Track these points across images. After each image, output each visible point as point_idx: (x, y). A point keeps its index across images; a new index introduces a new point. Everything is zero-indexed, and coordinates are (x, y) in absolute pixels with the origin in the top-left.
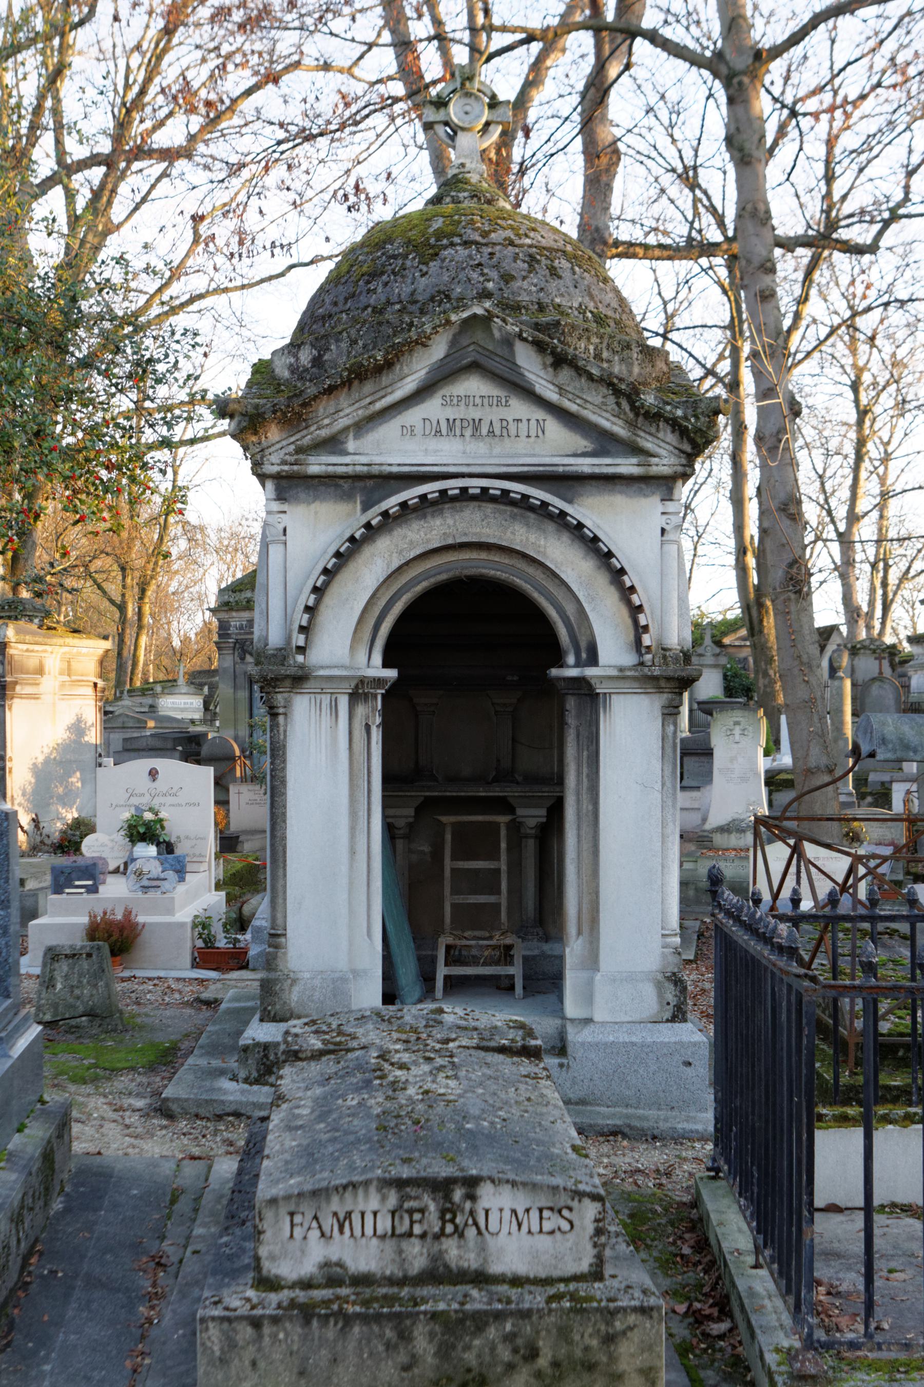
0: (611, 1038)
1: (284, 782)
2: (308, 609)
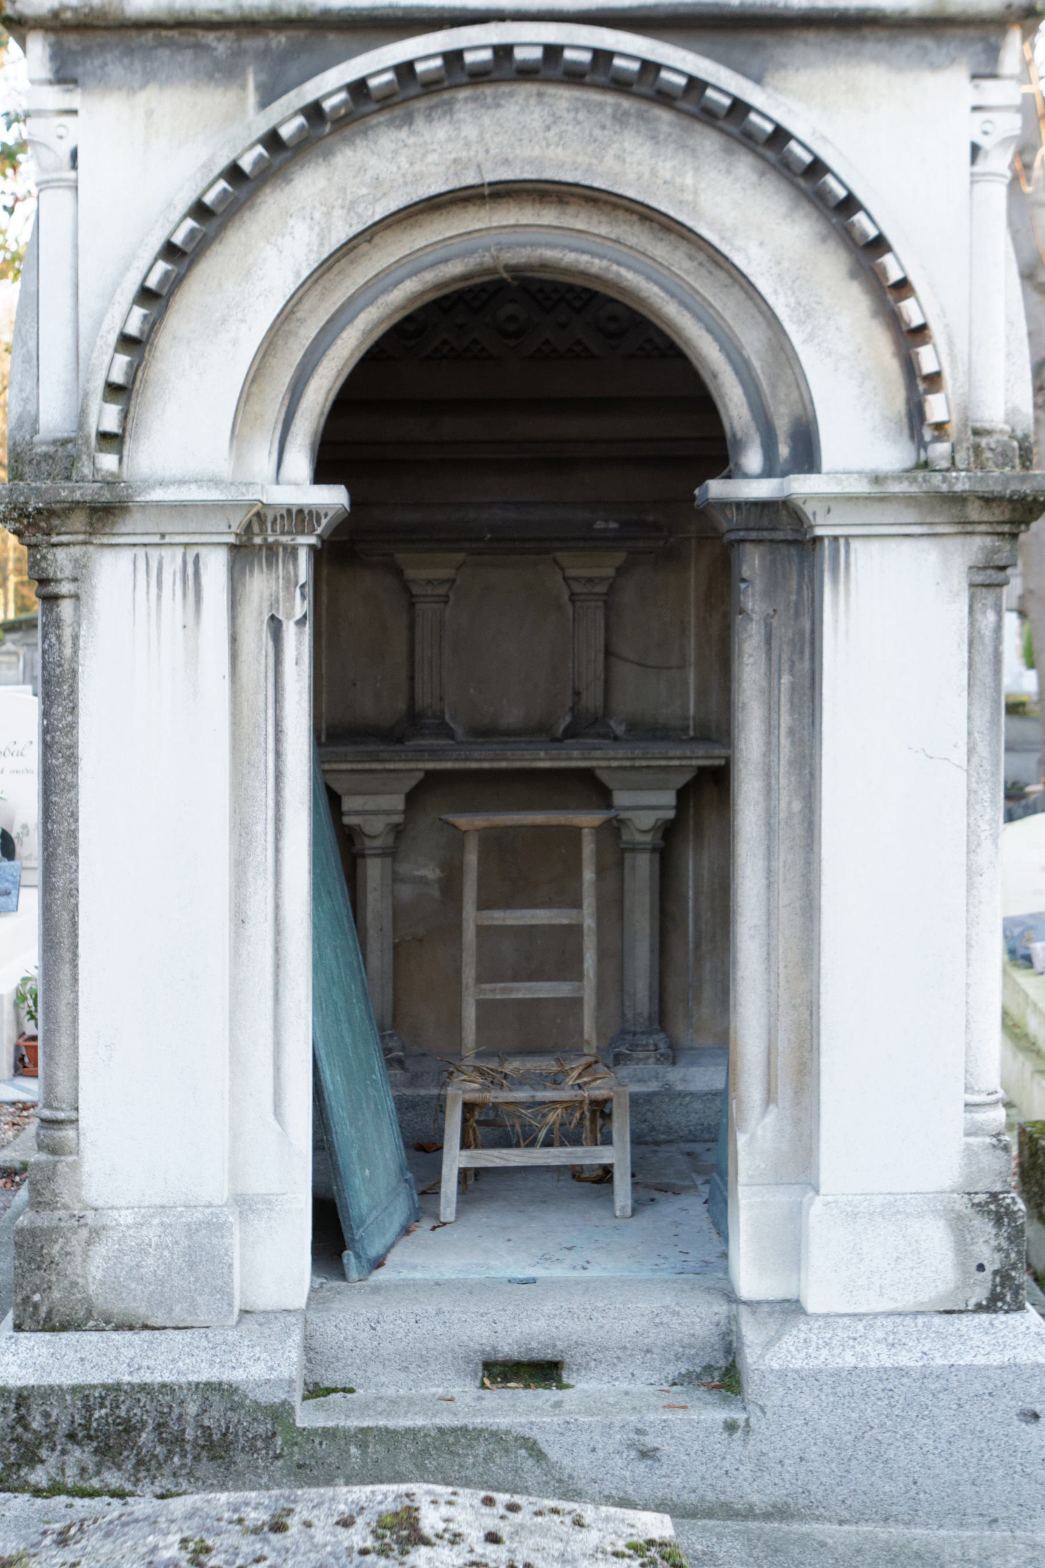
0: (849, 1360)
1: (72, 760)
2: (127, 342)
